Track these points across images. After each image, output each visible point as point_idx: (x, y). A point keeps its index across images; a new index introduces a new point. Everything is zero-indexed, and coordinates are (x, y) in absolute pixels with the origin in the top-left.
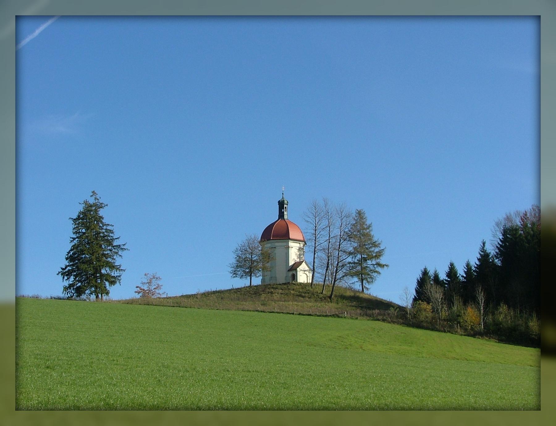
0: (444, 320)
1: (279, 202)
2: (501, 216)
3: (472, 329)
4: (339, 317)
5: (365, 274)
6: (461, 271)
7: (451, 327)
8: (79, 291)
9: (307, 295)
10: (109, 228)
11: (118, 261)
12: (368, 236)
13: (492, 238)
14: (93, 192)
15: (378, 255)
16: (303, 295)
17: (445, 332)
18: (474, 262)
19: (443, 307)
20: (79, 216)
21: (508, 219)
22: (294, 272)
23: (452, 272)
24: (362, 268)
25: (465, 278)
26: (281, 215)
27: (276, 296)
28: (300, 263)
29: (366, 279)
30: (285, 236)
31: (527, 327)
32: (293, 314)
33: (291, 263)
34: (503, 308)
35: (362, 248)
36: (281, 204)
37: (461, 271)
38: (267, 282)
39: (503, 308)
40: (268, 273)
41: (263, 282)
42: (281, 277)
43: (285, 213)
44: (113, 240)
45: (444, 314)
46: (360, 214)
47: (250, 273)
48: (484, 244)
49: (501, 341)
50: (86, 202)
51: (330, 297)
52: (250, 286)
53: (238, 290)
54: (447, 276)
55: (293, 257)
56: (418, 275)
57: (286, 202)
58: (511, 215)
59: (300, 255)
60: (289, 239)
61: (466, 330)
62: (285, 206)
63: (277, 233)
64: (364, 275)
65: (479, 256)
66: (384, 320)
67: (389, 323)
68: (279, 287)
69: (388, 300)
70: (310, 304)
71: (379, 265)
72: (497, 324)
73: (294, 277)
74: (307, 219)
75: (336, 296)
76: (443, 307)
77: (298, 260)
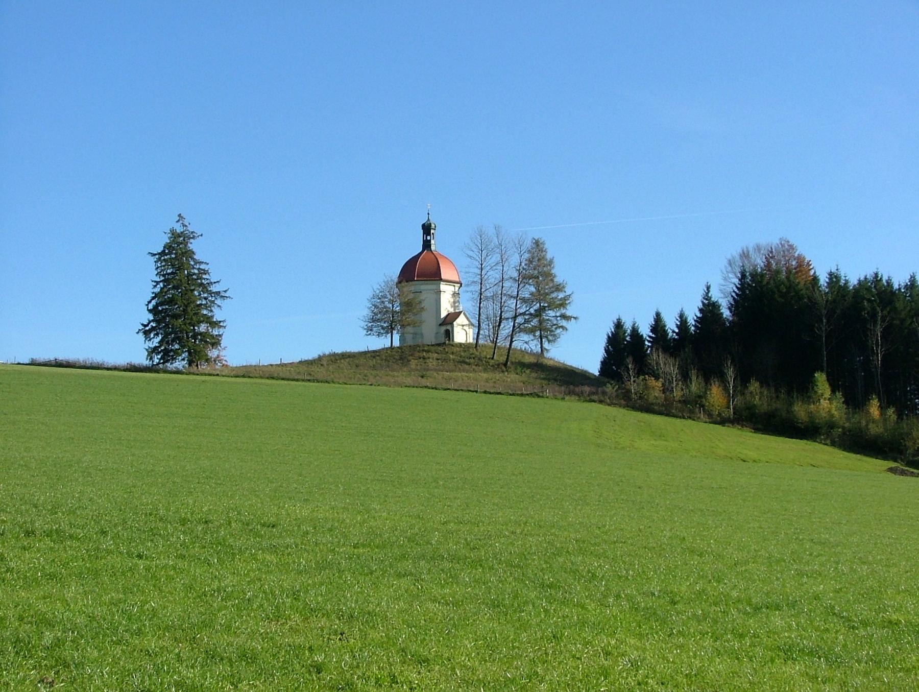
0: (680, 401)
1: (423, 226)
2: (734, 251)
3: (720, 414)
4: (539, 396)
5: (546, 330)
6: (671, 325)
7: (691, 411)
8: (168, 356)
9: (472, 361)
10: (202, 267)
11: (218, 315)
12: (549, 276)
13: (722, 282)
14: (179, 215)
15: (563, 304)
16: (467, 360)
17: (684, 418)
18: (692, 314)
19: (677, 384)
20: (164, 251)
21: (745, 255)
22: (449, 327)
23: (658, 326)
24: (540, 322)
25: (677, 334)
26: (427, 245)
27: (432, 363)
28: (456, 315)
29: (546, 337)
30: (435, 276)
31: (789, 412)
32: (476, 392)
33: (443, 314)
34: (754, 386)
35: (541, 294)
36: (427, 229)
37: (671, 325)
38: (410, 342)
39: (754, 386)
40: (409, 329)
41: (411, 340)
42: (429, 333)
43: (432, 242)
44: (210, 284)
45: (677, 394)
46: (537, 243)
47: (390, 329)
48: (708, 288)
49: (757, 430)
50: (173, 232)
51: (505, 365)
52: (392, 348)
53: (375, 354)
54: (652, 331)
55: (446, 308)
56: (609, 328)
57: (433, 226)
58: (748, 252)
59: (454, 302)
60: (441, 280)
61: (710, 415)
62: (432, 231)
63: (421, 271)
64: (545, 332)
65: (701, 305)
66: (601, 402)
67: (609, 405)
68: (433, 348)
69: (809, 442)
70: (485, 375)
71: (564, 317)
72: (750, 408)
73: (449, 334)
74: (471, 253)
75: (512, 363)
76: (677, 384)
77: (452, 310)
